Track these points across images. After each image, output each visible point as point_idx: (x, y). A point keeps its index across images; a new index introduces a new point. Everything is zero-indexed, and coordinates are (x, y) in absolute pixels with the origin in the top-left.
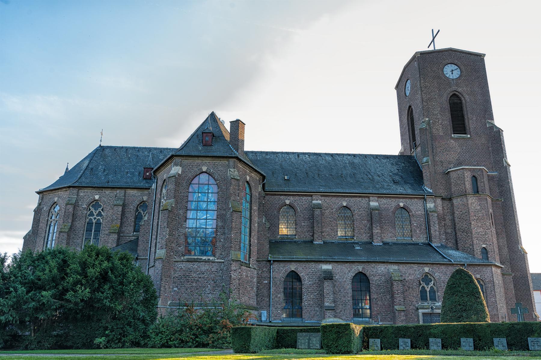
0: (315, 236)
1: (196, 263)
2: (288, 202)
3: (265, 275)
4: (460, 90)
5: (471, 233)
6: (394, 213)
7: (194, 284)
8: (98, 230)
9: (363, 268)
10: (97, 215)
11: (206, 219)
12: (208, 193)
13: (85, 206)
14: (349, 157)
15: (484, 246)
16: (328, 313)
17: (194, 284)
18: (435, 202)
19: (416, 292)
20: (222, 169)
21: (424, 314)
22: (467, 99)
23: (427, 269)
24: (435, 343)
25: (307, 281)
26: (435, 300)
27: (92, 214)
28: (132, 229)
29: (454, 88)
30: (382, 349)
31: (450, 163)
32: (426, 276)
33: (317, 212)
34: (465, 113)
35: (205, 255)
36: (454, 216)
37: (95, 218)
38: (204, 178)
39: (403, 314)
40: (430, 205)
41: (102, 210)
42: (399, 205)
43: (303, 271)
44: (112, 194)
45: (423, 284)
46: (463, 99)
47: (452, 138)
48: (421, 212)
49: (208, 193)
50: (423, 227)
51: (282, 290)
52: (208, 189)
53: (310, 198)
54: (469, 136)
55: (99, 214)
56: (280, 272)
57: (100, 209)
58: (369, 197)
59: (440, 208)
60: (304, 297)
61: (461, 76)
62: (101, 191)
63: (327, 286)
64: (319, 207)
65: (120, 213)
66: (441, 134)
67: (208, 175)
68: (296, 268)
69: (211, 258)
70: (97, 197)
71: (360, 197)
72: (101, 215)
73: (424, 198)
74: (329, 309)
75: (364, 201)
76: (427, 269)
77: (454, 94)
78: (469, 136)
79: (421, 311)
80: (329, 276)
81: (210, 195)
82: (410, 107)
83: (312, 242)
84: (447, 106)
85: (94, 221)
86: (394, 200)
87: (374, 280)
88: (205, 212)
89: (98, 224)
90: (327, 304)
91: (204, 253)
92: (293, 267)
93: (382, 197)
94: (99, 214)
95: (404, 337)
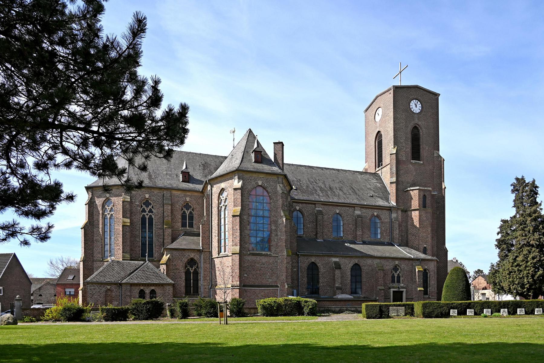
0: (318, 235)
1: (258, 257)
2: (298, 208)
3: (295, 264)
4: (420, 123)
5: (419, 237)
6: (370, 220)
7: (258, 272)
8: (151, 224)
9: (358, 261)
10: (149, 212)
11: (263, 224)
12: (263, 203)
13: (137, 203)
14: (334, 172)
15: (425, 246)
16: (338, 291)
17: (258, 272)
18: (397, 213)
19: (389, 278)
20: (273, 184)
21: (394, 292)
22: (423, 133)
23: (397, 262)
24: (453, 312)
25: (322, 270)
26: (400, 282)
27: (144, 211)
28: (180, 224)
29: (416, 121)
30: (406, 315)
31: (408, 183)
32: (396, 266)
33: (320, 217)
34: (421, 143)
35: (264, 251)
36: (407, 224)
37: (147, 214)
38: (260, 190)
39: (382, 291)
40: (394, 215)
41: (153, 207)
42: (374, 214)
43: (320, 263)
44: (160, 194)
45: (394, 272)
46: (421, 131)
47: (412, 163)
48: (388, 220)
49: (263, 203)
50: (388, 231)
51: (306, 275)
52: (263, 200)
53: (313, 206)
54: (422, 162)
55: (150, 211)
56: (304, 263)
57: (150, 207)
58: (354, 207)
59: (400, 218)
60: (321, 281)
61: (421, 111)
62: (150, 191)
63: (337, 272)
64: (320, 212)
65: (170, 211)
66: (404, 159)
67: (262, 188)
68: (315, 260)
69: (269, 253)
70: (147, 196)
71: (348, 206)
72: (152, 212)
73: (390, 210)
74: (338, 288)
75: (351, 210)
76: (397, 262)
77: (415, 127)
78: (422, 162)
79: (392, 290)
80: (338, 266)
81: (265, 205)
82: (379, 132)
83: (315, 240)
84: (409, 136)
85: (147, 217)
86: (371, 210)
87: (364, 269)
88: (262, 218)
89: (151, 219)
90: (337, 285)
91: (263, 249)
92: (313, 260)
93: (363, 208)
94: (150, 211)
95: (453, 308)
